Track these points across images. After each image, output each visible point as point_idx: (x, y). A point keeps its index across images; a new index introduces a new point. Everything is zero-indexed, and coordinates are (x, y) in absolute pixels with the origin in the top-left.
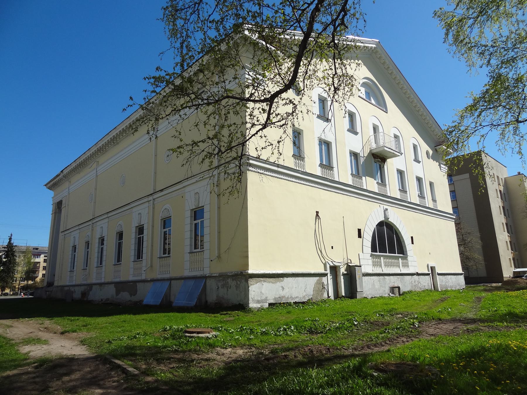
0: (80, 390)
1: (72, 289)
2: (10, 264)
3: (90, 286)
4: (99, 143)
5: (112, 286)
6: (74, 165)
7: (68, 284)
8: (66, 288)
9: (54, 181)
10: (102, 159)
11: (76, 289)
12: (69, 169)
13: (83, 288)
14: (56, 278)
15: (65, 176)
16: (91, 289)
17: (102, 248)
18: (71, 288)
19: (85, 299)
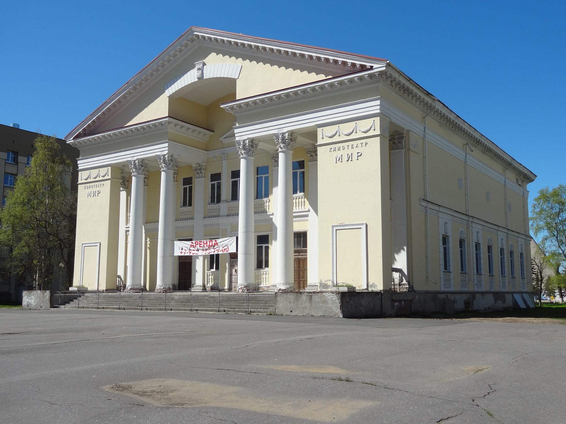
0: (194, 165)
1: (451, 297)
2: (66, 226)
3: (473, 294)
4: (484, 138)
5: (491, 295)
6: (452, 117)
7: (443, 289)
8: (442, 296)
9: (411, 87)
10: (477, 152)
11: (457, 297)
12: (444, 111)
13: (465, 297)
14: (204, 75)
15: (431, 108)
16: (474, 298)
17: (476, 251)
18: (449, 295)
19: (470, 309)
